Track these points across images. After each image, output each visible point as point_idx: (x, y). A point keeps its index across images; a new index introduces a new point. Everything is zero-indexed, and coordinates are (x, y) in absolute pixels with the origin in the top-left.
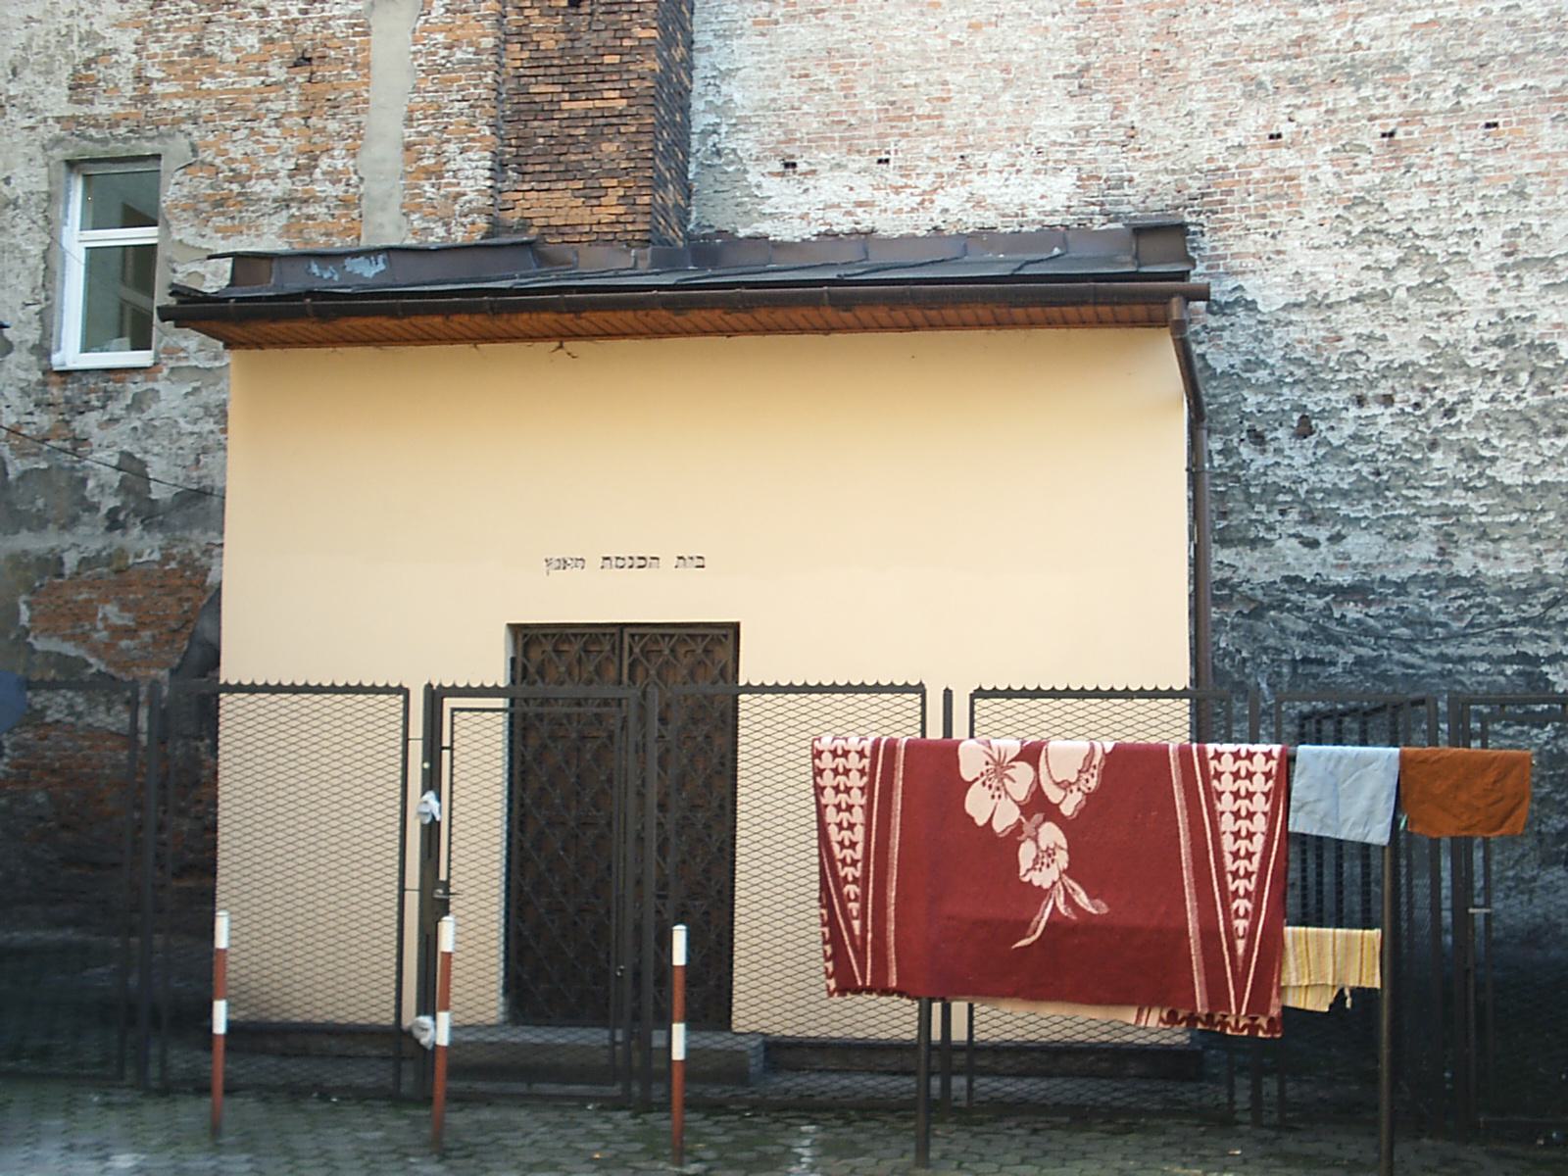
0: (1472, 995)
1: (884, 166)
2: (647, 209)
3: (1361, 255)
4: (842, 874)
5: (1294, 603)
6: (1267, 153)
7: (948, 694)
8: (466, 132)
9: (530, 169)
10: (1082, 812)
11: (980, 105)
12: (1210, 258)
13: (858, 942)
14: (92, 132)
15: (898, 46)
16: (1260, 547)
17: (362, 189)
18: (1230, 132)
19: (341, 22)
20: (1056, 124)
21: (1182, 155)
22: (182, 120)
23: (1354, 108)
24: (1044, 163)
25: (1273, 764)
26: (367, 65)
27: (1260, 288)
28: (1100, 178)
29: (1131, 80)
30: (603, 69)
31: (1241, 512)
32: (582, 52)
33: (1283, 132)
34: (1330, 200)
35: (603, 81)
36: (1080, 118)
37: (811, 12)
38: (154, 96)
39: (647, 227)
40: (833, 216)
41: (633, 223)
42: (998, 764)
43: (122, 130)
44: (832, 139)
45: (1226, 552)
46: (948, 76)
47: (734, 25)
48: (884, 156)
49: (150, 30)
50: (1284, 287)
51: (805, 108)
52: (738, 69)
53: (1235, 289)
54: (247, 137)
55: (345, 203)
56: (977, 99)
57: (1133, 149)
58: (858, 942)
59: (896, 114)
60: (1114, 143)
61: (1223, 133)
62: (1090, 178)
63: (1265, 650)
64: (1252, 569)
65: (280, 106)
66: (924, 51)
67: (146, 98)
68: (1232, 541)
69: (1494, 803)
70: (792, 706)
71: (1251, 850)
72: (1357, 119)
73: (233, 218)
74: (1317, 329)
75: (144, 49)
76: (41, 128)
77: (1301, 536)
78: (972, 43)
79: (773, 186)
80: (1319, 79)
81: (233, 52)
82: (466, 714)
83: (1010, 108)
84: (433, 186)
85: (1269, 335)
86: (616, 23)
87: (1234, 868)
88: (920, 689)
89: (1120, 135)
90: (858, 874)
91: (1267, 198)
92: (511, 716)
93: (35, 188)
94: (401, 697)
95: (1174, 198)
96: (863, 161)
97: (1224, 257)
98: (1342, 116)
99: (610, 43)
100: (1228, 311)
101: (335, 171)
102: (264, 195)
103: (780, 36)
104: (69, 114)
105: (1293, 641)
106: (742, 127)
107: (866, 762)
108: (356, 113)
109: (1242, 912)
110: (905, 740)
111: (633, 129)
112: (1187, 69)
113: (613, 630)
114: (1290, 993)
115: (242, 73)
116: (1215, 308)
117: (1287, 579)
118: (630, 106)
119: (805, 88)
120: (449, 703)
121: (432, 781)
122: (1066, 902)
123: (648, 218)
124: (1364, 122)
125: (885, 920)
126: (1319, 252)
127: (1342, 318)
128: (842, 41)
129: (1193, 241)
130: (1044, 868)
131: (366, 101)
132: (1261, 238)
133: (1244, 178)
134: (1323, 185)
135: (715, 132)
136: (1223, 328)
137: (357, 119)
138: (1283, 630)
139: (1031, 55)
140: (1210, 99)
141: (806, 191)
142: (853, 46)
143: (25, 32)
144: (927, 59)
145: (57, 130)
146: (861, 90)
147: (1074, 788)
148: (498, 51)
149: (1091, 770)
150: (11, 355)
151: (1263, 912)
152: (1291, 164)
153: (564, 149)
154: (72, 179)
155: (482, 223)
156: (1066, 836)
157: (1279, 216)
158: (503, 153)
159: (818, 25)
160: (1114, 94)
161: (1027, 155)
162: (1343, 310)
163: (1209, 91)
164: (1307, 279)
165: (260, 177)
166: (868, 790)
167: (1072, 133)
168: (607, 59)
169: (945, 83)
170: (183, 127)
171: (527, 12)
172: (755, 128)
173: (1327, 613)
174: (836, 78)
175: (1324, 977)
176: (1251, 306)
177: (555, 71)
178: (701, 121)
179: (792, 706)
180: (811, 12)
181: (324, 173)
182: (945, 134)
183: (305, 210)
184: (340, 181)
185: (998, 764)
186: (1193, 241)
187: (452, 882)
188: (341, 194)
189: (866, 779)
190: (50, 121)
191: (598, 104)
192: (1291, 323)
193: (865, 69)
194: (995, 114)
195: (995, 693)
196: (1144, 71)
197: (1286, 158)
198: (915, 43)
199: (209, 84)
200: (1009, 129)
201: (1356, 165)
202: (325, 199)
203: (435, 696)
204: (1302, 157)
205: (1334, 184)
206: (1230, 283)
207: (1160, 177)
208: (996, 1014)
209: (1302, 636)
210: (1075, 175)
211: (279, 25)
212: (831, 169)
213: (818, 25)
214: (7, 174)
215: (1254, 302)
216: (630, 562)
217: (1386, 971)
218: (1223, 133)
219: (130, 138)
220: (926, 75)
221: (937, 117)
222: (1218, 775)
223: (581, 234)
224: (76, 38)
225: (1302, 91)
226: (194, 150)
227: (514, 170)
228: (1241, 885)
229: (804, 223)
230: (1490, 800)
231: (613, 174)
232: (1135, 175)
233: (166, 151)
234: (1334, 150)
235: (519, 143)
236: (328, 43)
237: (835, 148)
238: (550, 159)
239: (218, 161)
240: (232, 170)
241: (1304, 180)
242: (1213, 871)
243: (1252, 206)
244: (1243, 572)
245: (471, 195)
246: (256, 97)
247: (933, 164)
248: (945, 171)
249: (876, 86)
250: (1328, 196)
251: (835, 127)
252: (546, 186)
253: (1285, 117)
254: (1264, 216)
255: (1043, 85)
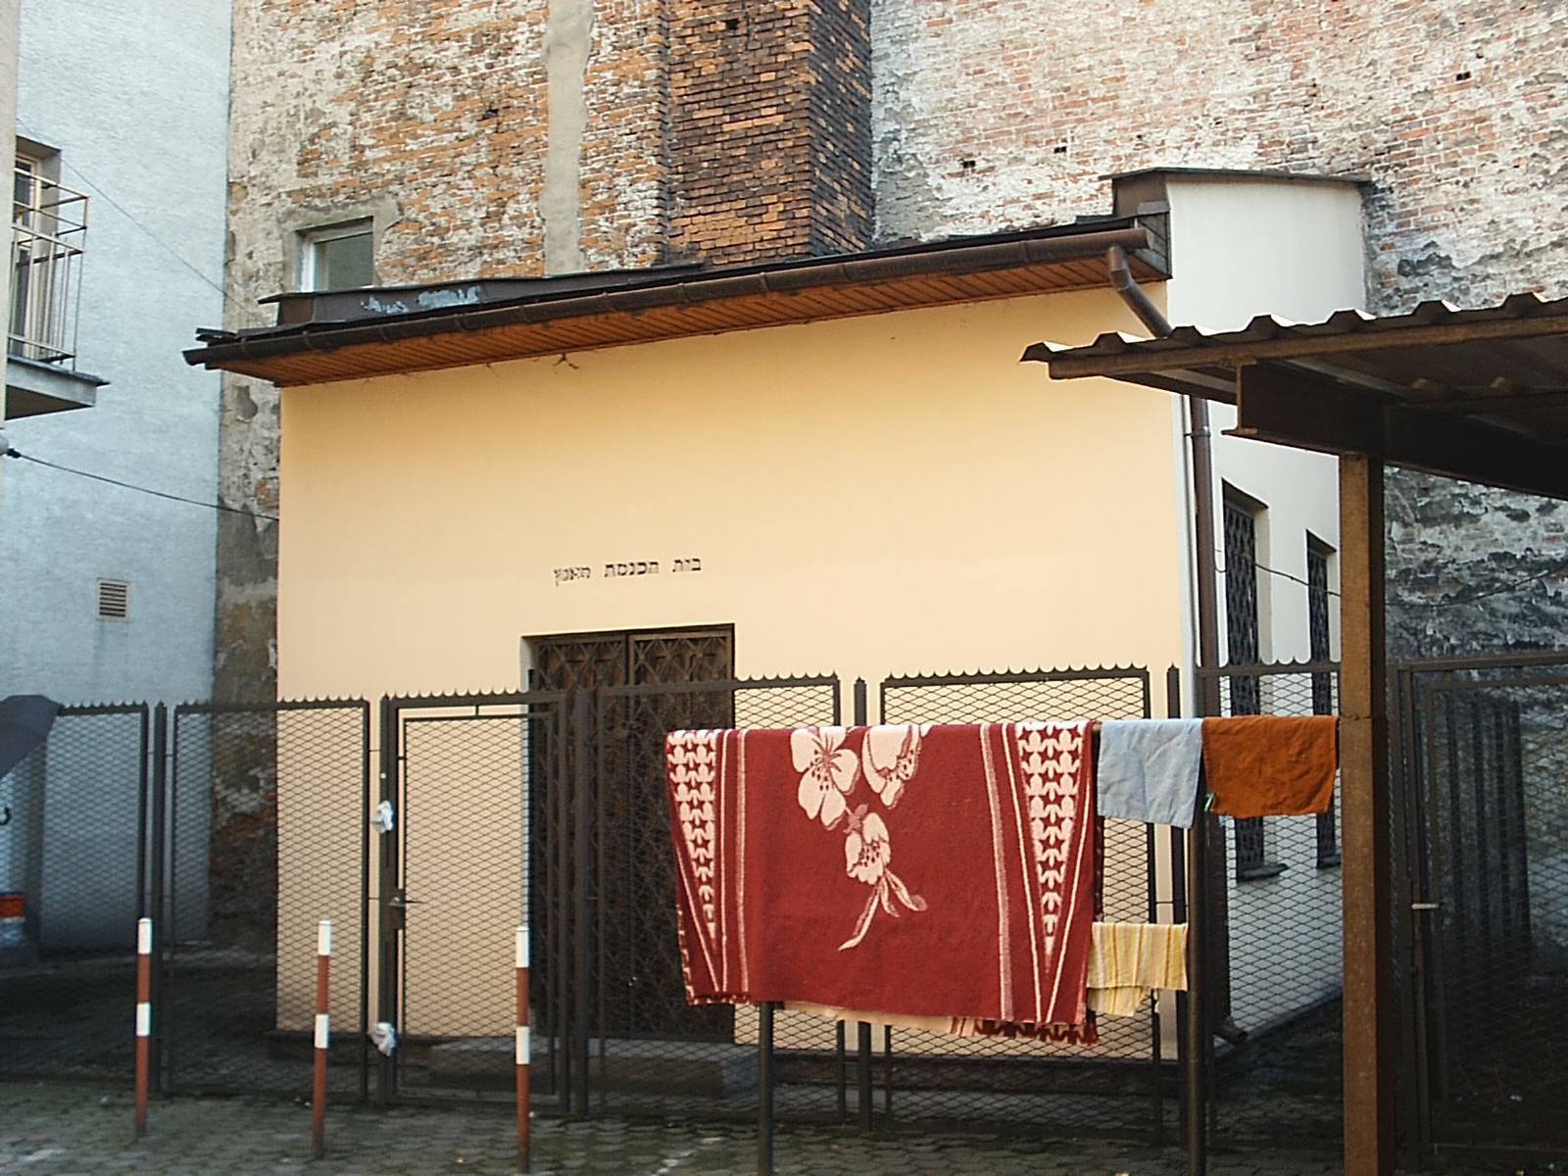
0: (1421, 1004)
1: (1061, 155)
2: (805, 222)
3: (1560, 194)
4: (697, 874)
5: (1504, 583)
6: (1455, 96)
7: (860, 687)
8: (633, 164)
9: (696, 194)
10: (901, 800)
11: (1155, 81)
12: (1400, 216)
13: (714, 946)
14: (317, 202)
15: (1071, 30)
16: (1465, 524)
17: (545, 230)
18: (1416, 77)
19: (522, 72)
20: (1235, 91)
21: (1366, 108)
22: (390, 182)
23: (1547, 34)
24: (1223, 134)
25: (1079, 741)
26: (546, 111)
27: (1453, 242)
28: (1282, 143)
29: (1310, 36)
30: (759, 87)
31: (1443, 487)
32: (740, 73)
33: (1471, 70)
34: (1525, 139)
35: (761, 99)
36: (1258, 82)
37: (983, 6)
38: (366, 162)
39: (806, 240)
40: (1013, 211)
41: (793, 237)
42: (826, 752)
43: (341, 198)
44: (1009, 133)
45: (1430, 531)
46: (1122, 55)
47: (910, 30)
48: (1061, 145)
49: (362, 101)
50: (1479, 238)
51: (981, 104)
52: (915, 73)
53: (1427, 246)
54: (445, 192)
55: (530, 245)
56: (1152, 74)
57: (1316, 108)
58: (714, 946)
59: (1071, 100)
60: (1295, 105)
61: (1408, 79)
62: (1272, 144)
63: (1475, 635)
64: (1458, 549)
65: (471, 159)
66: (1097, 31)
67: (359, 165)
68: (1435, 519)
69: (1301, 776)
70: (754, 701)
71: (1060, 837)
72: (1551, 46)
73: (435, 270)
74: (1517, 281)
75: (358, 119)
76: (276, 203)
77: (1509, 508)
78: (1145, 17)
79: (952, 187)
80: (1508, 8)
81: (432, 113)
82: (417, 724)
83: (1185, 80)
84: (607, 220)
85: (1466, 292)
86: (770, 40)
87: (1044, 859)
88: (833, 681)
89: (1301, 95)
90: (711, 874)
91: (1457, 144)
92: (531, 721)
93: (272, 259)
94: (361, 710)
95: (1360, 155)
96: (1040, 153)
97: (1414, 213)
98: (1534, 45)
99: (766, 60)
100: (1421, 271)
101: (521, 215)
102: (460, 245)
103: (953, 35)
104: (298, 187)
105: (1505, 624)
106: (921, 131)
107: (713, 755)
108: (537, 158)
109: (1051, 907)
110: (745, 731)
111: (790, 144)
112: (1368, 15)
113: (622, 638)
114: (1101, 996)
115: (440, 131)
116: (1408, 269)
117: (1494, 556)
118: (786, 121)
119: (980, 84)
120: (404, 713)
121: (390, 791)
122: (889, 899)
123: (807, 231)
124: (1558, 48)
125: (737, 922)
126: (1516, 196)
127: (1544, 265)
128: (1014, 32)
129: (1382, 199)
130: (870, 862)
131: (545, 145)
132: (1452, 188)
133: (1431, 126)
134: (1517, 122)
135: (895, 139)
136: (1416, 290)
137: (538, 163)
138: (1493, 612)
139: (1205, 22)
140: (1392, 45)
141: (985, 188)
142: (1025, 35)
143: (262, 117)
144: (1098, 40)
145: (289, 204)
146: (1035, 79)
147: (894, 775)
148: (662, 82)
149: (909, 755)
150: (258, 416)
151: (1072, 906)
152: (1482, 104)
153: (727, 171)
154: (304, 247)
155: (651, 251)
156: (887, 827)
157: (1471, 162)
158: (671, 181)
159: (990, 19)
160: (1293, 52)
161: (1206, 128)
162: (1544, 257)
163: (1392, 36)
164: (1503, 227)
165: (457, 228)
166: (715, 785)
167: (1251, 99)
168: (764, 77)
169: (1119, 62)
170: (391, 188)
171: (689, 40)
172: (934, 130)
173: (1541, 591)
174: (1010, 70)
175: (1130, 979)
176: (1445, 263)
177: (716, 94)
178: (881, 129)
179: (754, 701)
180: (983, 6)
181: (511, 218)
182: (1121, 115)
183: (496, 256)
184: (525, 224)
185: (826, 752)
186: (1382, 199)
187: (408, 890)
188: (526, 236)
189: (713, 773)
190: (283, 196)
191: (757, 122)
192: (1488, 277)
193: (1038, 57)
194: (1172, 88)
195: (906, 682)
196: (1324, 24)
197: (1476, 98)
198: (1087, 25)
199: (412, 145)
200: (1186, 102)
201: (1551, 97)
202: (513, 243)
203: (391, 707)
204: (1493, 95)
205: (1527, 120)
206: (1422, 240)
207: (1344, 135)
208: (803, 1017)
209: (1514, 618)
210: (1256, 143)
211: (469, 82)
212: (1009, 163)
213: (990, 19)
214: (251, 248)
215: (1448, 258)
216: (630, 569)
217: (1192, 971)
218: (1408, 79)
219: (347, 205)
220: (1100, 56)
221: (1112, 98)
222: (1027, 755)
223: (745, 253)
224: (302, 117)
225: (1490, 23)
226: (401, 210)
227: (681, 196)
228: (1051, 876)
229: (985, 222)
230: (1297, 772)
231: (773, 190)
232: (1319, 135)
233: (377, 212)
234: (1526, 83)
235: (686, 169)
236: (512, 94)
237: (1011, 141)
238: (714, 182)
239: (421, 218)
240: (433, 224)
241: (1496, 119)
242: (1024, 861)
243: (1442, 154)
244: (1448, 552)
245: (641, 225)
246: (452, 153)
247: (1110, 148)
248: (1122, 153)
249: (1050, 73)
250: (1523, 134)
251: (1012, 121)
252: (711, 209)
253: (1473, 54)
254: (1455, 164)
255: (1218, 51)
